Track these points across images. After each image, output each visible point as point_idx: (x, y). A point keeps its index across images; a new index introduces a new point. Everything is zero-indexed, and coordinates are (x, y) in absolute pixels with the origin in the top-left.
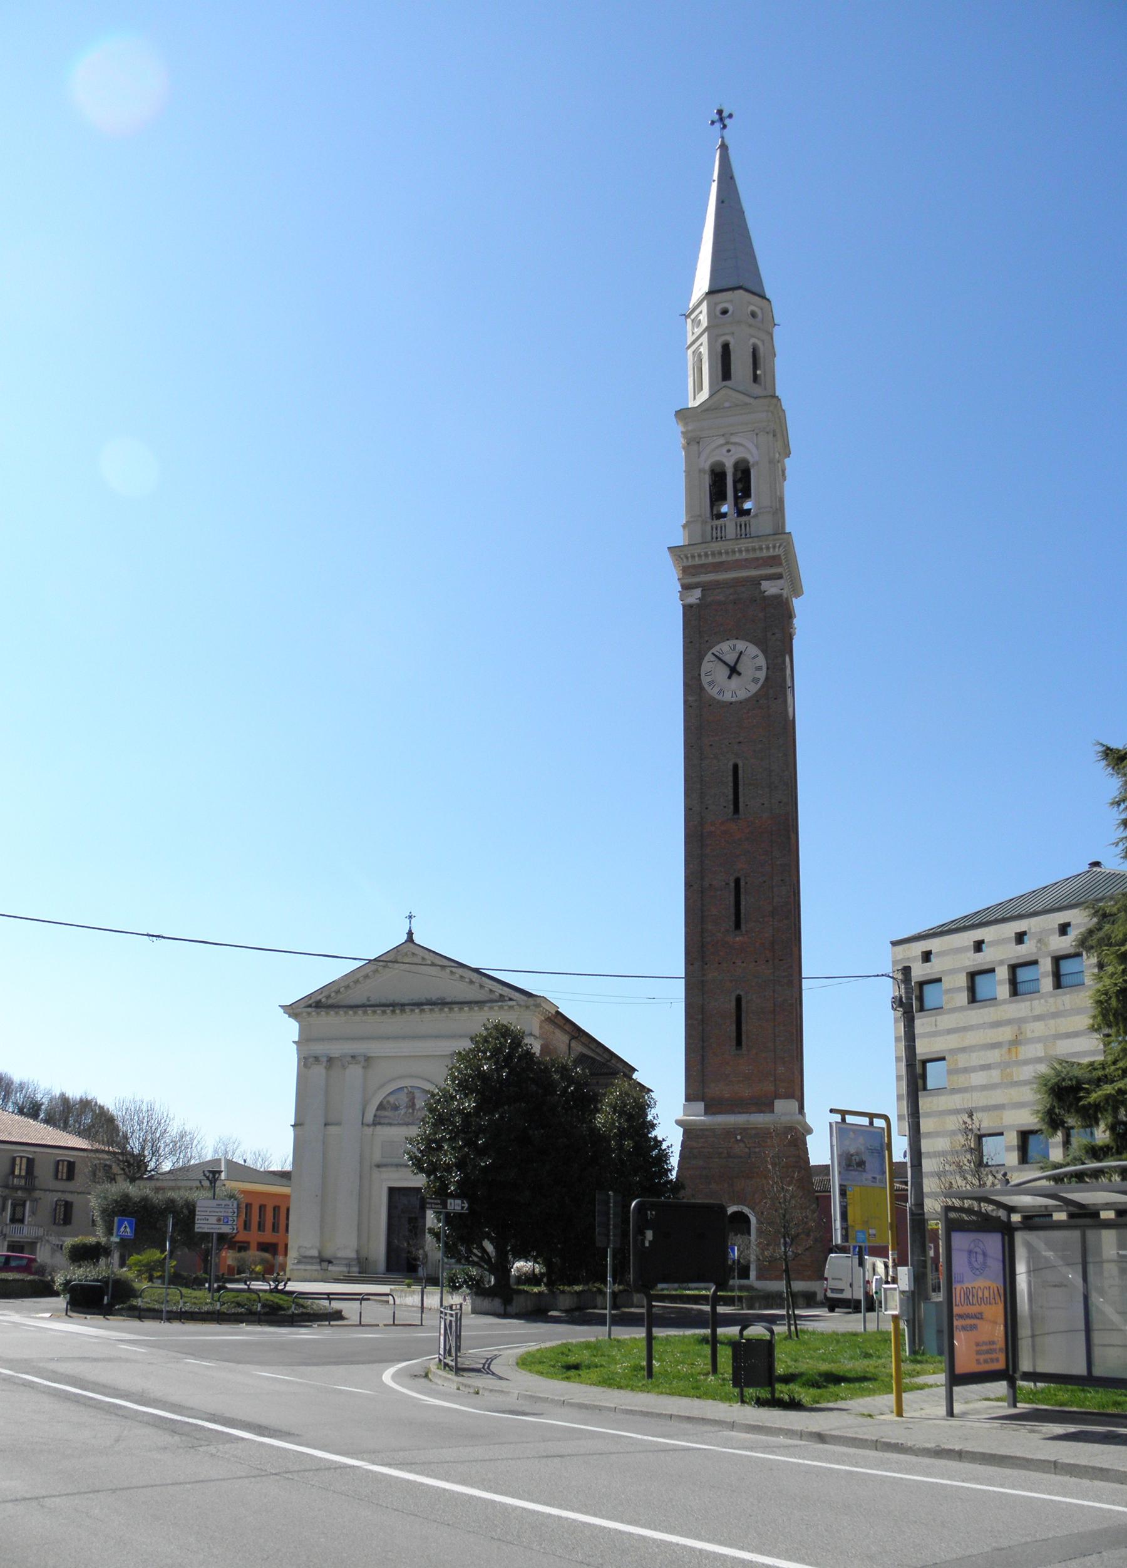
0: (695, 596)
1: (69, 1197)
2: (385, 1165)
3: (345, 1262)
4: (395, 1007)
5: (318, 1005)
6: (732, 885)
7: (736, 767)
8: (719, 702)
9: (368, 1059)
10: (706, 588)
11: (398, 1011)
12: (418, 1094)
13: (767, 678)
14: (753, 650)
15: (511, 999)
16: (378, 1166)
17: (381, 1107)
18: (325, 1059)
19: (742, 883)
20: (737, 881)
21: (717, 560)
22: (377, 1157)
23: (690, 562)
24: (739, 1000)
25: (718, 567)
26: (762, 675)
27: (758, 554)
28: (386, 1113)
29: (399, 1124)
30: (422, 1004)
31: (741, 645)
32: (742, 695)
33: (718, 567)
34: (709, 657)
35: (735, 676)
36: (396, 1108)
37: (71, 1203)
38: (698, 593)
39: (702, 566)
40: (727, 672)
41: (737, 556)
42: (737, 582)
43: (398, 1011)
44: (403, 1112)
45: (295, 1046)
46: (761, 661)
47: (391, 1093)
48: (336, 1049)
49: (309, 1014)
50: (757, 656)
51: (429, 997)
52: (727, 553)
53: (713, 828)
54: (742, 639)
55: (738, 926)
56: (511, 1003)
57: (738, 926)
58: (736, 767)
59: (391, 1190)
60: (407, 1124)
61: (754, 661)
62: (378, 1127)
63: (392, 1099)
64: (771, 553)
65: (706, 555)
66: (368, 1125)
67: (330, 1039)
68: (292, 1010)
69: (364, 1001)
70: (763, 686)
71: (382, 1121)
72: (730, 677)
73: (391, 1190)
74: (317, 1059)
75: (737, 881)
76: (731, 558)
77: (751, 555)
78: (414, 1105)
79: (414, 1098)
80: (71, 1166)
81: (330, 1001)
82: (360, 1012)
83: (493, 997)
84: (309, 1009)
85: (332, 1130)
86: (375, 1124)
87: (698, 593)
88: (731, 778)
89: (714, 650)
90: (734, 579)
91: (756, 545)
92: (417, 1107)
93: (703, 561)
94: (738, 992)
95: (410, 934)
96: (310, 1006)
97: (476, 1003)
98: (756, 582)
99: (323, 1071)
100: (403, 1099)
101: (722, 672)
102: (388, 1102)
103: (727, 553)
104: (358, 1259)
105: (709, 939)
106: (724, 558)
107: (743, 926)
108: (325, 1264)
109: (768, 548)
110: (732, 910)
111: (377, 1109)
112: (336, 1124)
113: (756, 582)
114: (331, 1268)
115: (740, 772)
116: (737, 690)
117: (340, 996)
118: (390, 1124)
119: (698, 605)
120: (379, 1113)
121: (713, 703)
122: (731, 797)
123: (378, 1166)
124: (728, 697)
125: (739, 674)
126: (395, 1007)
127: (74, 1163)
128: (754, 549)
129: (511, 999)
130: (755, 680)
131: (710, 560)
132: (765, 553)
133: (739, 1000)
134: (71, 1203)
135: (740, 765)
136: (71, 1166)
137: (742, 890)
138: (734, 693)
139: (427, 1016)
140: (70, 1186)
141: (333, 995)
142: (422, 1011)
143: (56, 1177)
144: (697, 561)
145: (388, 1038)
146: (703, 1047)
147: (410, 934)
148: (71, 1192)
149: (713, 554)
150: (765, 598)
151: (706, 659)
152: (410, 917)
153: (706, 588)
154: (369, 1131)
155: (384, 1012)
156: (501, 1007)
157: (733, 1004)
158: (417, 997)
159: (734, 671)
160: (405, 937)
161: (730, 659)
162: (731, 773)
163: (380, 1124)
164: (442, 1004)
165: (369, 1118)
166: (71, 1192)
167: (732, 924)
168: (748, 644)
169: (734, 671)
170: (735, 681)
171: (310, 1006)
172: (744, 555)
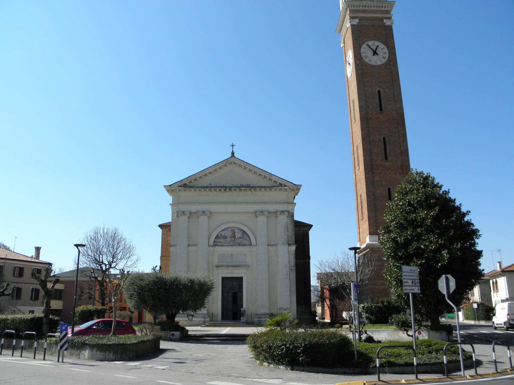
0: (356, 22)
1: (19, 286)
2: (221, 266)
3: (202, 316)
4: (225, 188)
5: (185, 186)
6: (382, 140)
7: (379, 92)
8: (369, 65)
9: (211, 213)
10: (361, 19)
11: (228, 190)
12: (236, 231)
13: (389, 57)
14: (382, 46)
15: (285, 186)
16: (217, 266)
17: (217, 237)
18: (188, 213)
19: (387, 140)
20: (384, 139)
21: (364, 9)
22: (216, 262)
23: (352, 8)
24: (389, 189)
25: (364, 11)
26: (387, 56)
27: (381, 9)
28: (220, 240)
29: (227, 245)
30: (266, 187)
31: (377, 43)
32: (379, 63)
33: (364, 11)
34: (364, 46)
35: (376, 55)
36: (225, 238)
37: (21, 289)
38: (357, 21)
39: (358, 10)
40: (372, 53)
41: (372, 8)
42: (372, 19)
43: (228, 190)
44: (229, 239)
45: (170, 207)
46: (386, 50)
47: (223, 230)
48: (194, 208)
49: (179, 190)
50: (383, 48)
51: (242, 184)
52: (377, 7)
53: (372, 116)
54: (377, 41)
55: (386, 158)
56: (285, 187)
57: (386, 158)
58: (379, 92)
59: (223, 279)
60: (232, 246)
61: (383, 50)
62: (217, 247)
63: (223, 233)
64: (386, 9)
65: (374, 7)
66: (211, 246)
67: (191, 203)
68: (170, 189)
69: (208, 185)
70: (388, 60)
71: (218, 244)
72: (374, 55)
73: (223, 279)
74: (183, 212)
75: (384, 139)
76: (370, 9)
77: (378, 9)
78: (235, 236)
79: (234, 233)
80: (21, 270)
81: (191, 184)
82: (208, 190)
83: (275, 184)
84: (180, 188)
85: (192, 248)
86: (214, 245)
87: (357, 21)
88: (378, 96)
89: (367, 43)
90: (371, 17)
91: (381, 5)
92: (237, 237)
93: (358, 8)
94: (389, 187)
95: (233, 153)
96: (181, 186)
97: (268, 187)
98: (382, 20)
99: (187, 219)
100: (229, 233)
101: (370, 53)
102: (221, 235)
103: (368, 6)
104: (208, 314)
105: (374, 163)
106: (367, 8)
107: (389, 158)
108: (190, 317)
109: (385, 7)
110: (383, 151)
111: (215, 238)
112: (194, 246)
113: (382, 20)
114: (194, 319)
115: (381, 94)
116: (378, 60)
117: (196, 182)
118: (223, 246)
119: (357, 25)
120: (216, 240)
121: (366, 64)
122: (378, 104)
123: (217, 266)
124: (373, 63)
125: (378, 54)
126: (225, 188)
127: (23, 268)
128: (379, 7)
129: (285, 186)
130: (384, 58)
131: (361, 8)
132: (383, 9)
133: (389, 189)
134: (21, 289)
135: (381, 91)
136: (21, 270)
137: (387, 143)
138: (375, 62)
139: (242, 193)
140: (20, 280)
141: (193, 181)
142: (240, 190)
143: (14, 276)
144: (355, 8)
145: (222, 203)
146: (375, 211)
147: (233, 153)
148: (21, 283)
149: (363, 6)
150: (385, 26)
151: (363, 47)
152: (233, 146)
153: (361, 19)
154: (212, 249)
155: (220, 190)
156: (281, 190)
157: (387, 191)
158: (239, 184)
159: (375, 53)
160: (231, 155)
161: (374, 48)
162: (377, 94)
163: (217, 245)
164: (249, 187)
165: (211, 242)
166: (21, 283)
167: (384, 157)
168: (379, 43)
169: (375, 53)
170: (375, 58)
171: (181, 186)
172: (375, 8)
